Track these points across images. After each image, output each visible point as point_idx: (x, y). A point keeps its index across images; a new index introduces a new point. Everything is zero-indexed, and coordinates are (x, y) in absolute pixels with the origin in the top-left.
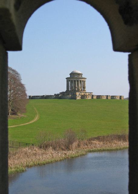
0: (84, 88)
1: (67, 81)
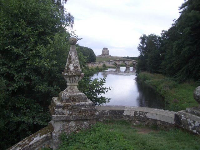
0: (108, 53)
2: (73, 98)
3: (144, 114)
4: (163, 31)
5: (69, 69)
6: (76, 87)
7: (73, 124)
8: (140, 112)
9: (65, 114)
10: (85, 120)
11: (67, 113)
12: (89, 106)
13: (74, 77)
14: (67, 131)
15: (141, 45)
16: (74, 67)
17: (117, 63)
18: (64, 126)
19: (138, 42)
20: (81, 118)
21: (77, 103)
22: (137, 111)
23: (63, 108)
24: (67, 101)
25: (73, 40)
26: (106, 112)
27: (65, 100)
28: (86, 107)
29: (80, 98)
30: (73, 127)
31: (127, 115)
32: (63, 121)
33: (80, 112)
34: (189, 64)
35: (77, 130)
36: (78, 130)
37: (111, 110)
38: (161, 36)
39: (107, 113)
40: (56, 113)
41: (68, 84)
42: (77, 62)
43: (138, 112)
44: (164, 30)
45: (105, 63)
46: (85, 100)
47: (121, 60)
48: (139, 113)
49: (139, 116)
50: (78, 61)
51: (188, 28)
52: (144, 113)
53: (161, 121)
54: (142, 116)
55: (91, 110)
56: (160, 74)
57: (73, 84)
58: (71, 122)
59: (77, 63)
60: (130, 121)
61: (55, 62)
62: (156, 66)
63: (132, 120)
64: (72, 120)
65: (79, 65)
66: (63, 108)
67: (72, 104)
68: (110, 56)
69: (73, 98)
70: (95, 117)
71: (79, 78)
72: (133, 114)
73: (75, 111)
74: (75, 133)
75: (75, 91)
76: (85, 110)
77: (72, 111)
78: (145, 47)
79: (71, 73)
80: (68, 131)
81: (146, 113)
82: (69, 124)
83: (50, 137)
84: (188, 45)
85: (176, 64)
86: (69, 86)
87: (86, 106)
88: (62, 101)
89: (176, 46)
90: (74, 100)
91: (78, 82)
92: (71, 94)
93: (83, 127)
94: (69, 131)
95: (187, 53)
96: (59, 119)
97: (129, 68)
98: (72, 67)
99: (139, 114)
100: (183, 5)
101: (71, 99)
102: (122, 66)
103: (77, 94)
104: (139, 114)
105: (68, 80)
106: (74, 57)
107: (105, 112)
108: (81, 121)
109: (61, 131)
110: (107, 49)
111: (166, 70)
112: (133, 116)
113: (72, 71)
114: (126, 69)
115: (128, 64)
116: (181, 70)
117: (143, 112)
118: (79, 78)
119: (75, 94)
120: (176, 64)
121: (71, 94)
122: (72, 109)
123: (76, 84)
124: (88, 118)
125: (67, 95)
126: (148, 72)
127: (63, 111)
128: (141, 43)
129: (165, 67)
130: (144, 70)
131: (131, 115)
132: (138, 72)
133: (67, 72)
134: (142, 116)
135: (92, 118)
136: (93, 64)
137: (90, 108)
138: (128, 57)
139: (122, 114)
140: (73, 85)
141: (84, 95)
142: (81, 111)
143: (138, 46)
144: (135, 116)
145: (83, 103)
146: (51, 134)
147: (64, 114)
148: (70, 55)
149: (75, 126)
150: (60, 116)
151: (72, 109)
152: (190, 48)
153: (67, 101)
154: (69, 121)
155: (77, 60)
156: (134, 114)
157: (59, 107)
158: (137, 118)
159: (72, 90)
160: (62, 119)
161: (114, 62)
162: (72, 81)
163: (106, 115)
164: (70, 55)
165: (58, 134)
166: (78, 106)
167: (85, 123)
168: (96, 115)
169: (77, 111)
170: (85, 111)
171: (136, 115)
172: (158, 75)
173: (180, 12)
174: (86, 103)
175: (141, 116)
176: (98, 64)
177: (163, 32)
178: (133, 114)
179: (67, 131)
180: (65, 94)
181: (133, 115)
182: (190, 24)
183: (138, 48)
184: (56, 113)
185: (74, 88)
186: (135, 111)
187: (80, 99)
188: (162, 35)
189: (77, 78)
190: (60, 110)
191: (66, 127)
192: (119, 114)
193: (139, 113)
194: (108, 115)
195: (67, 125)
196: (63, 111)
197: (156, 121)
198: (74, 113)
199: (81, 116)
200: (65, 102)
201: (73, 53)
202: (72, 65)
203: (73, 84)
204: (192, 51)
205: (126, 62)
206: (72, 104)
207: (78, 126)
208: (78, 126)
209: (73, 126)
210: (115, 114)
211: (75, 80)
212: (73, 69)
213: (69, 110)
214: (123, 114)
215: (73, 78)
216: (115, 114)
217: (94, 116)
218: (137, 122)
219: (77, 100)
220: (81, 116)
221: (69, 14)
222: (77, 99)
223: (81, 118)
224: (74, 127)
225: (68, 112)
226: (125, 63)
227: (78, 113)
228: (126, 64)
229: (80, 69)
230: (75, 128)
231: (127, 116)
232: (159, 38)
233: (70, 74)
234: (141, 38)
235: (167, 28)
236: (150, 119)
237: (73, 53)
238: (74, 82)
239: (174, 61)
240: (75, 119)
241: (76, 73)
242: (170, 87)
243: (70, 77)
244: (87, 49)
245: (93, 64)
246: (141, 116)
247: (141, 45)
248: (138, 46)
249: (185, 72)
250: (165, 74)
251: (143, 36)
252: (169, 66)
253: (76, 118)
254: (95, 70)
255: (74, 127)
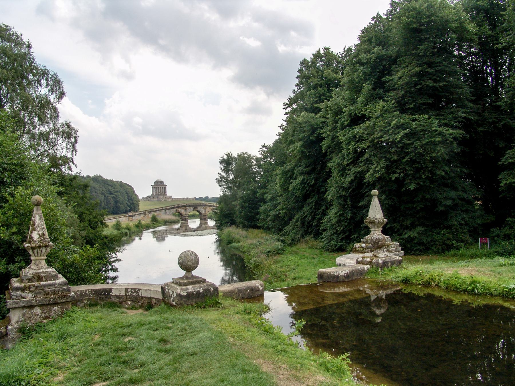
0: (165, 192)
1: (153, 188)
2: (37, 276)
3: (137, 292)
4: (263, 146)
5: (31, 238)
6: (44, 262)
7: (38, 310)
8: (132, 289)
9: (26, 298)
10: (55, 304)
11: (29, 296)
12: (61, 285)
13: (40, 249)
14: (29, 321)
15: (223, 174)
16: (39, 235)
17: (182, 211)
18: (24, 315)
19: (217, 170)
20: (49, 301)
21: (42, 283)
22: (128, 289)
23: (23, 290)
24: (30, 280)
25: (36, 200)
26: (87, 292)
27: (26, 280)
28: (57, 287)
29: (48, 276)
30: (38, 315)
31: (115, 295)
32: (23, 307)
33: (48, 294)
34: (305, 209)
35: (44, 319)
36: (46, 318)
37: (94, 290)
38: (260, 156)
39: (89, 294)
40: (13, 297)
41: (32, 258)
42: (44, 228)
43: (129, 290)
44: (266, 144)
45: (155, 214)
46: (55, 277)
47: (190, 206)
48: (131, 291)
49: (131, 295)
50: (45, 226)
51: (298, 144)
52: (136, 290)
53: (156, 299)
54: (135, 294)
55: (63, 291)
56: (259, 231)
57: (39, 258)
58: (35, 308)
59: (44, 230)
60: (121, 303)
61: (14, 230)
62: (253, 214)
63: (123, 301)
64: (36, 306)
65: (47, 233)
66: (23, 290)
67: (37, 284)
68: (170, 197)
69: (39, 277)
70: (69, 299)
71: (46, 250)
72: (123, 293)
73: (40, 293)
74: (41, 322)
75: (42, 267)
76: (55, 291)
77: (35, 293)
78: (231, 178)
79: (34, 243)
80: (30, 321)
81: (139, 290)
82: (32, 311)
83: (4, 334)
84: (301, 174)
85: (283, 209)
86: (33, 260)
87: (56, 286)
88: (22, 281)
89: (280, 176)
90: (40, 279)
91: (46, 255)
92: (35, 271)
93: (53, 313)
94: (33, 321)
95: (299, 189)
96: (17, 306)
97: (205, 219)
98: (35, 236)
99: (130, 292)
100: (290, 99)
101: (35, 278)
102: (193, 217)
103: (44, 271)
104: (130, 292)
105: (31, 252)
106: (40, 222)
107: (86, 292)
108: (49, 306)
109: (21, 321)
110: (162, 182)
111: (268, 222)
112: (124, 296)
113: (36, 241)
114: (201, 224)
115: (203, 212)
116: (294, 220)
117: (135, 289)
118: (46, 250)
119: (41, 271)
120: (283, 209)
121: (35, 271)
122: (36, 290)
123: (43, 258)
124: (59, 301)
125: (30, 272)
126: (238, 226)
127: (23, 294)
128: (222, 170)
129: (267, 215)
130: (233, 223)
131: (121, 295)
132: (220, 226)
133: (30, 242)
134: (135, 294)
135: (64, 301)
136: (132, 216)
137: (61, 288)
138: (207, 197)
139: (109, 294)
140: (39, 260)
141: (54, 271)
142: (48, 293)
143: (218, 177)
144: (126, 295)
145: (51, 282)
146: (6, 328)
147: (24, 298)
148: (34, 219)
149: (41, 314)
150: (18, 300)
151: (36, 290)
152: (304, 179)
153: (30, 280)
154: (31, 307)
155: (43, 225)
156: (124, 292)
157: (17, 289)
158: (129, 298)
159: (37, 265)
160: (22, 304)
161: (175, 209)
162: (36, 255)
163: (88, 296)
164: (34, 219)
165: (16, 326)
166: (44, 286)
167: (55, 308)
168: (70, 296)
169: (43, 293)
170: (54, 293)
171: (128, 294)
172: (256, 231)
173: (286, 114)
174: (57, 281)
175: (133, 294)
176: (142, 216)
177: (265, 149)
178: (123, 293)
179: (29, 321)
180: (28, 272)
181: (124, 294)
182: (301, 136)
183: (218, 181)
184: (13, 297)
185: (40, 263)
186: (126, 289)
187: (48, 278)
188: (261, 154)
189: (44, 250)
190: (19, 293)
191: (28, 316)
192: (105, 294)
193: (131, 291)
194: (90, 296)
195: (30, 312)
196: (23, 294)
197: (150, 298)
198: (38, 296)
199: (49, 298)
200: (27, 281)
201: (37, 216)
202: (36, 232)
203: (37, 258)
204: (308, 184)
205: (199, 208)
206: (37, 284)
207: (45, 313)
208: (45, 313)
209: (38, 313)
210: (100, 294)
211: (41, 252)
212: (37, 238)
213: (31, 292)
214: (111, 294)
215: (38, 250)
216: (100, 294)
217: (67, 299)
218: (129, 302)
219: (44, 279)
220: (49, 298)
221: (68, 125)
222: (44, 277)
223: (49, 301)
224: (40, 315)
225: (30, 295)
226: (198, 211)
227: (44, 295)
228: (200, 213)
229: (48, 237)
230: (41, 316)
231: (117, 296)
232: (257, 160)
233: (33, 245)
234: (222, 161)
235: (270, 142)
236: (144, 297)
237: (37, 216)
238: (39, 255)
239: (280, 203)
240: (40, 303)
241: (42, 243)
242: (269, 254)
243: (33, 249)
244: (121, 184)
245: (132, 216)
246: (133, 294)
247: (223, 174)
248: (218, 177)
249: (299, 223)
250: (267, 229)
251: (225, 157)
252: (273, 213)
253: (41, 302)
254: (134, 229)
255: (40, 315)
